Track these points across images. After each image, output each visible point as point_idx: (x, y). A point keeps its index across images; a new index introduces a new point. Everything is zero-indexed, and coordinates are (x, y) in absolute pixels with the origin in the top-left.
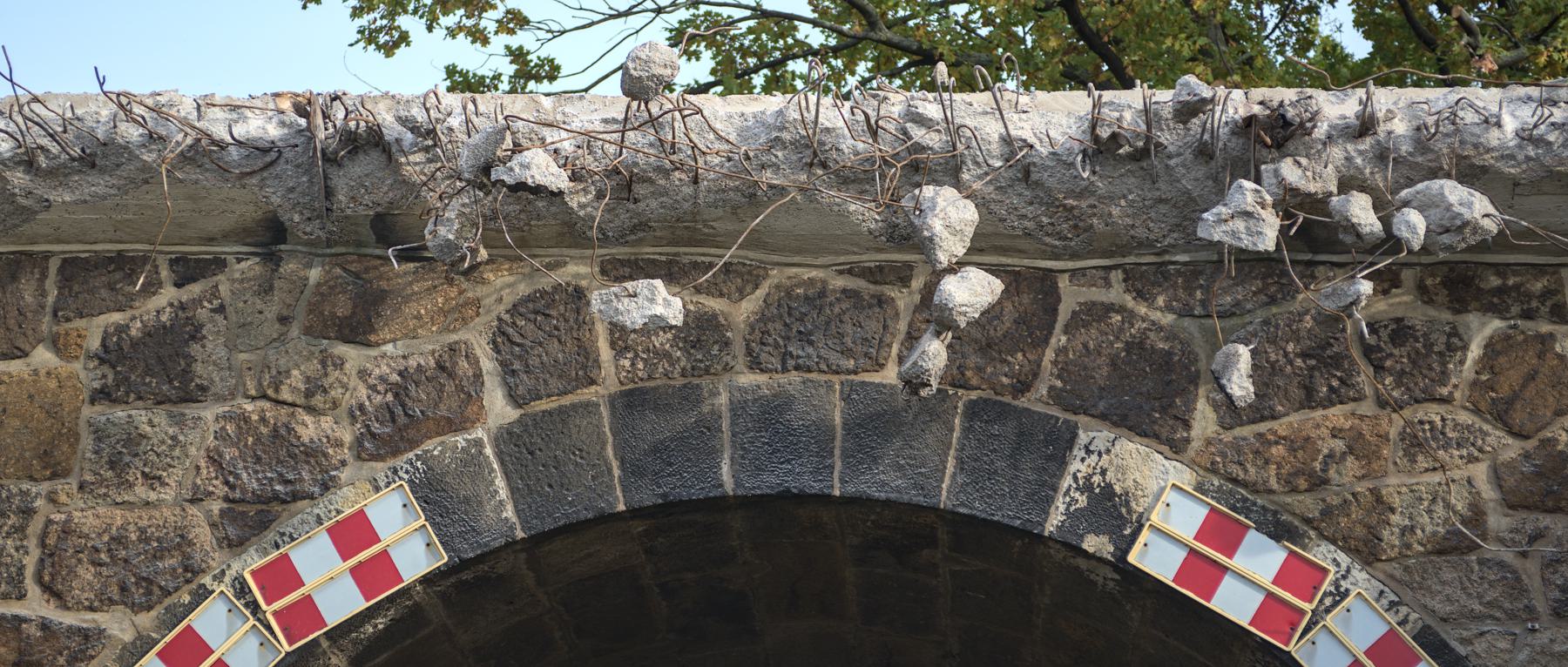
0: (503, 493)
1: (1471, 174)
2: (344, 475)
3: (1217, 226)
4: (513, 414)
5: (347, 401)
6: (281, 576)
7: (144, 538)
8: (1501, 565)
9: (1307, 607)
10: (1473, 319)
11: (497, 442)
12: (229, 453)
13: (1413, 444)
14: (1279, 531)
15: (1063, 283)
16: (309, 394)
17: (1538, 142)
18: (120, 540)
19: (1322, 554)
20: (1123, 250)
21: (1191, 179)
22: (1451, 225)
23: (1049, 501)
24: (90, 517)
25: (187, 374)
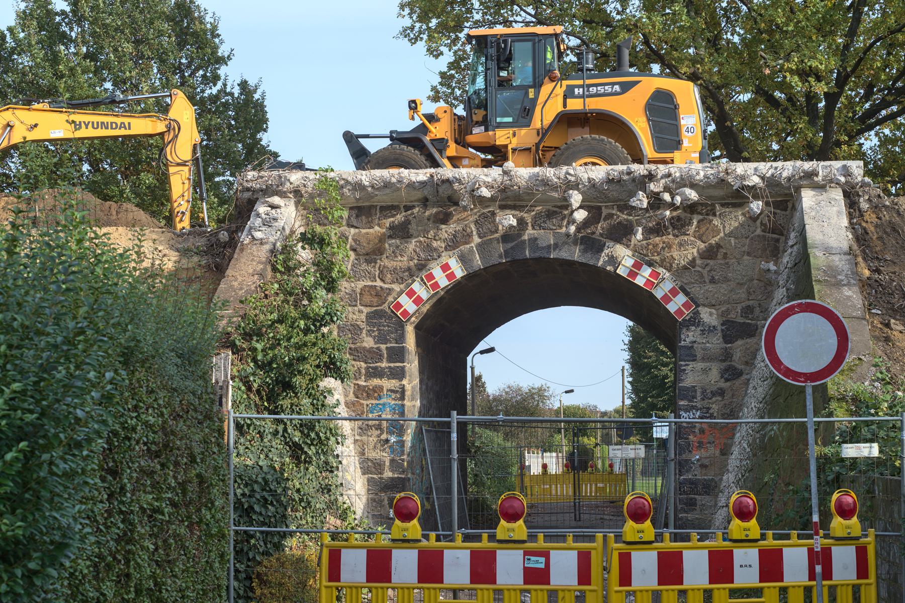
0: (478, 258)
1: (693, 186)
3: (634, 202)
4: (480, 240)
5: (443, 237)
6: (431, 277)
8: (699, 271)
10: (695, 216)
13: (681, 245)
14: (650, 264)
15: (603, 208)
16: (435, 236)
17: (708, 178)
18: (396, 269)
19: (660, 270)
22: (685, 199)
23: (599, 259)
25: (408, 232)
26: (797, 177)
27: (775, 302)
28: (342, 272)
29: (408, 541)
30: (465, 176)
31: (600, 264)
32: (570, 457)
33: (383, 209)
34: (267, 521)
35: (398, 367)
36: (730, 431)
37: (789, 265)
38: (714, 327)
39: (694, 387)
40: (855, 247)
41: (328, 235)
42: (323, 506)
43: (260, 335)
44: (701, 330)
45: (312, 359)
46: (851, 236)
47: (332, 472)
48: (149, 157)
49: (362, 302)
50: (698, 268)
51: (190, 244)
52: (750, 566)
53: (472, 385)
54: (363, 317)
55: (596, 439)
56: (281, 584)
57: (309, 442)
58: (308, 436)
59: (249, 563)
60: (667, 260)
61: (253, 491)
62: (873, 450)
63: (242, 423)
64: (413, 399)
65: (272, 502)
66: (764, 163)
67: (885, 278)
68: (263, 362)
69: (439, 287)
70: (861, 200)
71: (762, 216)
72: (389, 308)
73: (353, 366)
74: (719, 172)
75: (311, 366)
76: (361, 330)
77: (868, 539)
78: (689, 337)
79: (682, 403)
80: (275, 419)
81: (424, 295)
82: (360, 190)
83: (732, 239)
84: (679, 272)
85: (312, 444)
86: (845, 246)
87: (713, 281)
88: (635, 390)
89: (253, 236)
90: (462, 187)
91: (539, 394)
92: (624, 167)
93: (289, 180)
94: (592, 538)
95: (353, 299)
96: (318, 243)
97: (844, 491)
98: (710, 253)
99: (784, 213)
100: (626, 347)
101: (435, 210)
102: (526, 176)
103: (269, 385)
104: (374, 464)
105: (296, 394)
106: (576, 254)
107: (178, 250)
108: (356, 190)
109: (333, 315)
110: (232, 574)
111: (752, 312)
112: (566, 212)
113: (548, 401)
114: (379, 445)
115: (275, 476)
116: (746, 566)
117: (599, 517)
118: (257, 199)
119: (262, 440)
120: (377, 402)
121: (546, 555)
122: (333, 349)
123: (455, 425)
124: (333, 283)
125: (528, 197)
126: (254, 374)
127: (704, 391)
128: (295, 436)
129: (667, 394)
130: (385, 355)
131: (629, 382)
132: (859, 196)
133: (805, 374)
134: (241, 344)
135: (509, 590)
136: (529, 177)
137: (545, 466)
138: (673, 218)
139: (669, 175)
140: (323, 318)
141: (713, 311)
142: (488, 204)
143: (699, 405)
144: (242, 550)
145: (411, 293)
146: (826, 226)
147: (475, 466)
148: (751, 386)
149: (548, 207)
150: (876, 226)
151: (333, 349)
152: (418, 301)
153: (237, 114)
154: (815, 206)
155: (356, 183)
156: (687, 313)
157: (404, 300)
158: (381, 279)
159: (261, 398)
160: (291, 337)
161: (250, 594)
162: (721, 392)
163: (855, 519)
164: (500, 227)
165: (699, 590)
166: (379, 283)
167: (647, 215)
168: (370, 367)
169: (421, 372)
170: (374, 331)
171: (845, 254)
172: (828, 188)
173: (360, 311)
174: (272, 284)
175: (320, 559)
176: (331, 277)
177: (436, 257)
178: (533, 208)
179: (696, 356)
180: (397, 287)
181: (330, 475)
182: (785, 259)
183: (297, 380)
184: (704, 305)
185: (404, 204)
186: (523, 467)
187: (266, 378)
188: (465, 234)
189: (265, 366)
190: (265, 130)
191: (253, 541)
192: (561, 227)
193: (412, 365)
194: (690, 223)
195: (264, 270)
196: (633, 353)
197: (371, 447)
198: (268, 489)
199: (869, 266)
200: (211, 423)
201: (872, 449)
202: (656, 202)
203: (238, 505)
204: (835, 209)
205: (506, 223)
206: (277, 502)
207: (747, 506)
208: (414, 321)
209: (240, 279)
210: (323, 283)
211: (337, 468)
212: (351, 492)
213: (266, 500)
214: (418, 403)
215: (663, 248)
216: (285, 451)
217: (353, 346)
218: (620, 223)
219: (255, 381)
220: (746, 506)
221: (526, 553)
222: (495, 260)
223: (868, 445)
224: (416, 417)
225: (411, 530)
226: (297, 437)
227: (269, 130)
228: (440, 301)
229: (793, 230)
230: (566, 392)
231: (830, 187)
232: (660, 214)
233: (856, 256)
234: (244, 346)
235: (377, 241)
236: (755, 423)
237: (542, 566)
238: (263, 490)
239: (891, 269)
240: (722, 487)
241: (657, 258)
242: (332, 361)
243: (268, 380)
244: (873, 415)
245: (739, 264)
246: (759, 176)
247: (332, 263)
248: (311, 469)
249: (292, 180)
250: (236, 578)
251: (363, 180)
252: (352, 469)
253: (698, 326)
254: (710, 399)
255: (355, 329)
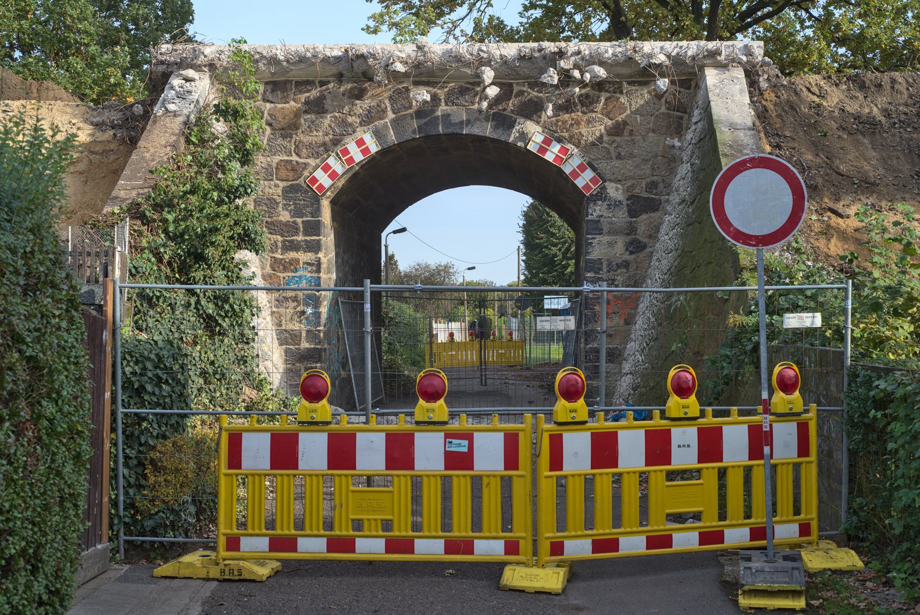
0: (392, 134)
1: (602, 64)
2: (358, 130)
3: (545, 79)
4: (394, 116)
5: (358, 113)
6: (346, 152)
7: (316, 143)
8: (606, 148)
9: (565, 157)
10: (603, 94)
11: (390, 122)
12: (333, 125)
13: (589, 122)
14: (559, 140)
15: (514, 85)
16: (349, 112)
17: (616, 56)
18: (311, 144)
19: (569, 146)
20: (527, 79)
21: (542, 64)
22: (594, 76)
23: (510, 135)
24: (306, 139)
25: (323, 107)
26: (700, 56)
27: (678, 177)
28: (256, 144)
29: (317, 423)
30: (380, 51)
31: (511, 139)
32: (472, 325)
33: (298, 84)
34: (161, 401)
35: (314, 240)
36: (634, 300)
37: (693, 141)
38: (620, 202)
39: (600, 259)
40: (758, 123)
41: (242, 107)
42: (239, 377)
43: (171, 206)
44: (608, 205)
45: (225, 230)
46: (753, 113)
47: (248, 343)
48: (78, 42)
49: (278, 177)
50: (605, 145)
51: (105, 118)
52: (689, 446)
53: (386, 263)
54: (279, 191)
55: (494, 310)
56: (177, 470)
57: (223, 314)
58: (222, 308)
59: (141, 449)
60: (576, 137)
61: (145, 368)
62: (815, 320)
63: (151, 295)
64: (329, 272)
65: (167, 381)
66: (670, 43)
67: (785, 153)
68: (175, 234)
69: (354, 162)
70: (761, 79)
71: (667, 94)
72: (305, 182)
73: (270, 239)
74: (626, 51)
75: (224, 237)
76: (278, 203)
77: (810, 415)
78: (596, 211)
79: (588, 275)
80: (188, 290)
81: (339, 170)
82: (275, 64)
83: (638, 116)
84: (588, 148)
85: (226, 316)
86: (749, 123)
87: (619, 157)
88: (528, 267)
89: (166, 108)
90: (378, 62)
91: (446, 270)
92: (536, 45)
93: (203, 53)
94: (518, 417)
95: (269, 174)
96: (232, 115)
97: (786, 364)
98: (616, 130)
99: (687, 91)
100: (521, 229)
101: (350, 86)
102: (440, 53)
103: (181, 256)
104: (291, 335)
105: (209, 266)
106: (487, 130)
107: (92, 124)
108: (271, 65)
109: (247, 187)
110: (121, 460)
111: (656, 187)
112: (478, 89)
113: (453, 277)
114: (296, 317)
115: (172, 352)
116: (684, 446)
117: (503, 381)
118: (172, 72)
119: (173, 312)
120: (293, 274)
121: (469, 437)
122: (247, 220)
123: (369, 294)
124: (247, 156)
125: (441, 74)
126: (164, 246)
127: (610, 264)
128: (208, 308)
129: (556, 271)
130: (301, 229)
131: (523, 260)
132: (759, 75)
133: (756, 237)
134: (151, 215)
135: (428, 476)
136: (443, 53)
137: (451, 335)
138: (581, 95)
139: (579, 53)
140: (237, 189)
141: (619, 186)
142: (402, 79)
143: (604, 277)
144: (132, 434)
145: (326, 168)
146: (730, 103)
147: (389, 335)
148: (655, 258)
149: (460, 84)
150: (775, 105)
151: (247, 220)
152: (333, 176)
153: (164, 4)
154: (719, 84)
155: (271, 57)
156: (594, 188)
157: (320, 174)
158: (297, 154)
159: (173, 270)
160: (204, 208)
161: (143, 482)
162: (626, 265)
163: (797, 393)
164: (414, 103)
165: (634, 472)
166: (294, 158)
167: (557, 92)
168: (286, 241)
169: (337, 246)
170: (290, 205)
171: (749, 129)
172: (730, 67)
173: (276, 186)
174: (185, 155)
175: (218, 444)
176: (246, 150)
177: (351, 132)
178: (446, 85)
179: (602, 230)
180: (312, 162)
181: (246, 347)
182: (689, 136)
183: (210, 252)
184: (610, 181)
185: (319, 79)
186: (432, 336)
187: (178, 249)
188: (380, 110)
189: (178, 238)
190: (191, 22)
191: (145, 424)
192: (473, 104)
193: (328, 239)
194: (598, 100)
195: (178, 141)
196: (527, 236)
197: (288, 318)
198: (162, 366)
199: (770, 142)
200: (56, 291)
201: (815, 319)
202: (566, 78)
203: (127, 384)
204: (738, 87)
205: (420, 98)
206: (173, 380)
207: (687, 382)
208: (330, 196)
209: (152, 150)
210: (237, 156)
211: (253, 340)
212: (268, 364)
213: (160, 378)
214: (334, 276)
215: (572, 125)
216: (199, 325)
217: (269, 220)
218: (530, 100)
219: (165, 252)
220: (685, 382)
221: (447, 436)
222: (408, 136)
223: (811, 314)
224: (332, 286)
225: (319, 412)
226: (211, 309)
227: (195, 22)
228: (355, 175)
229: (697, 108)
230: (469, 269)
231: (732, 66)
232: (570, 91)
233: (759, 132)
234: (155, 217)
235: (292, 116)
236: (660, 292)
237: (465, 450)
238: (156, 367)
239: (790, 145)
240: (625, 355)
241: (566, 135)
242: (247, 233)
243: (179, 251)
244: (788, 284)
245: (644, 140)
246: (665, 55)
247: (247, 136)
248: (226, 340)
249: (206, 53)
250: (126, 465)
251: (278, 54)
252: (269, 340)
253: (605, 200)
254: (616, 271)
255: (272, 203)
